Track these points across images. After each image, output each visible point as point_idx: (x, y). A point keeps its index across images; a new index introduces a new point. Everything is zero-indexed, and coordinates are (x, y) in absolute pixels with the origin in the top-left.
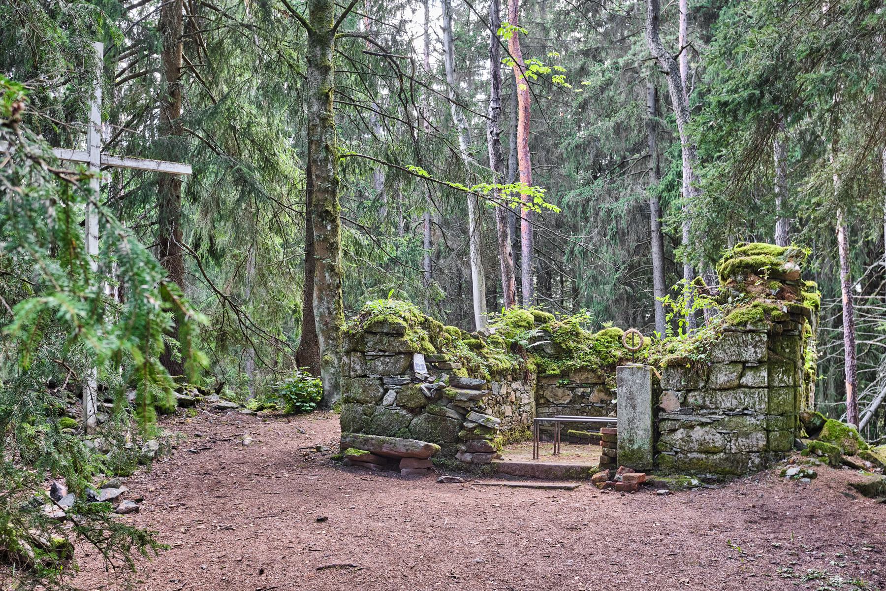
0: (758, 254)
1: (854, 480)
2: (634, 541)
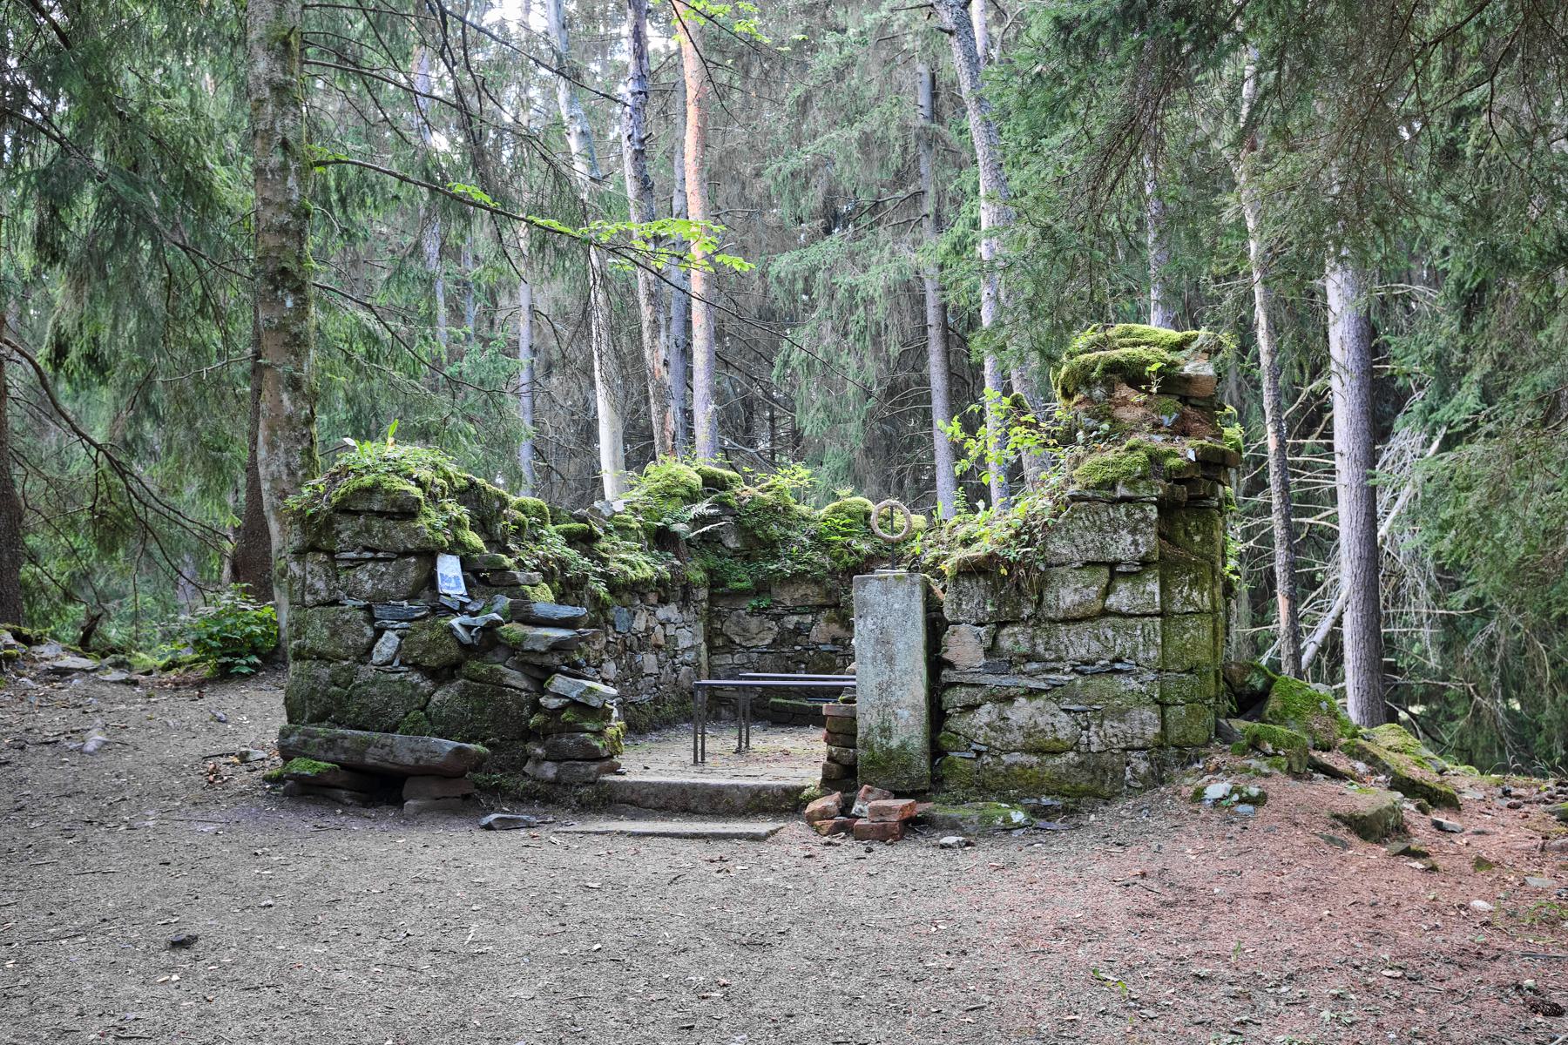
0: (1135, 345)
1: (1342, 807)
2: (888, 975)
